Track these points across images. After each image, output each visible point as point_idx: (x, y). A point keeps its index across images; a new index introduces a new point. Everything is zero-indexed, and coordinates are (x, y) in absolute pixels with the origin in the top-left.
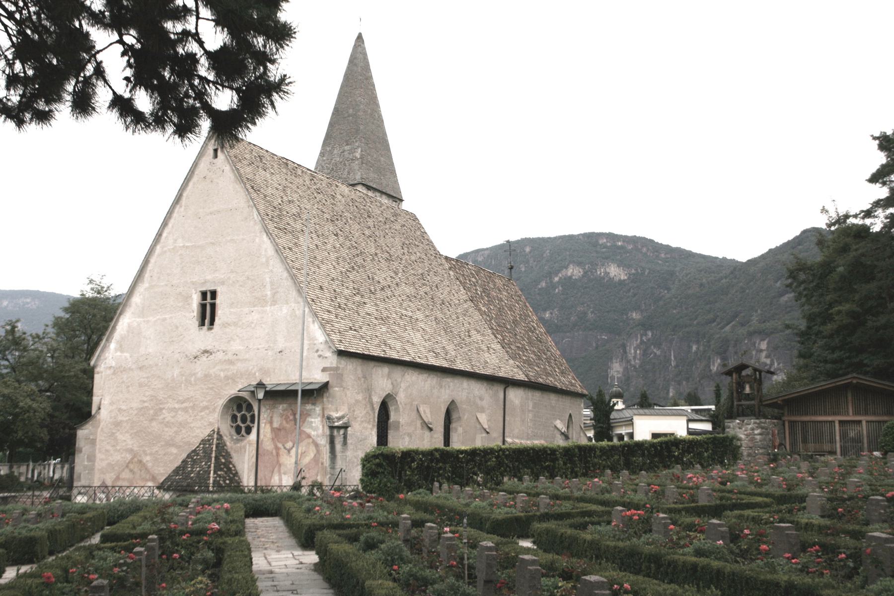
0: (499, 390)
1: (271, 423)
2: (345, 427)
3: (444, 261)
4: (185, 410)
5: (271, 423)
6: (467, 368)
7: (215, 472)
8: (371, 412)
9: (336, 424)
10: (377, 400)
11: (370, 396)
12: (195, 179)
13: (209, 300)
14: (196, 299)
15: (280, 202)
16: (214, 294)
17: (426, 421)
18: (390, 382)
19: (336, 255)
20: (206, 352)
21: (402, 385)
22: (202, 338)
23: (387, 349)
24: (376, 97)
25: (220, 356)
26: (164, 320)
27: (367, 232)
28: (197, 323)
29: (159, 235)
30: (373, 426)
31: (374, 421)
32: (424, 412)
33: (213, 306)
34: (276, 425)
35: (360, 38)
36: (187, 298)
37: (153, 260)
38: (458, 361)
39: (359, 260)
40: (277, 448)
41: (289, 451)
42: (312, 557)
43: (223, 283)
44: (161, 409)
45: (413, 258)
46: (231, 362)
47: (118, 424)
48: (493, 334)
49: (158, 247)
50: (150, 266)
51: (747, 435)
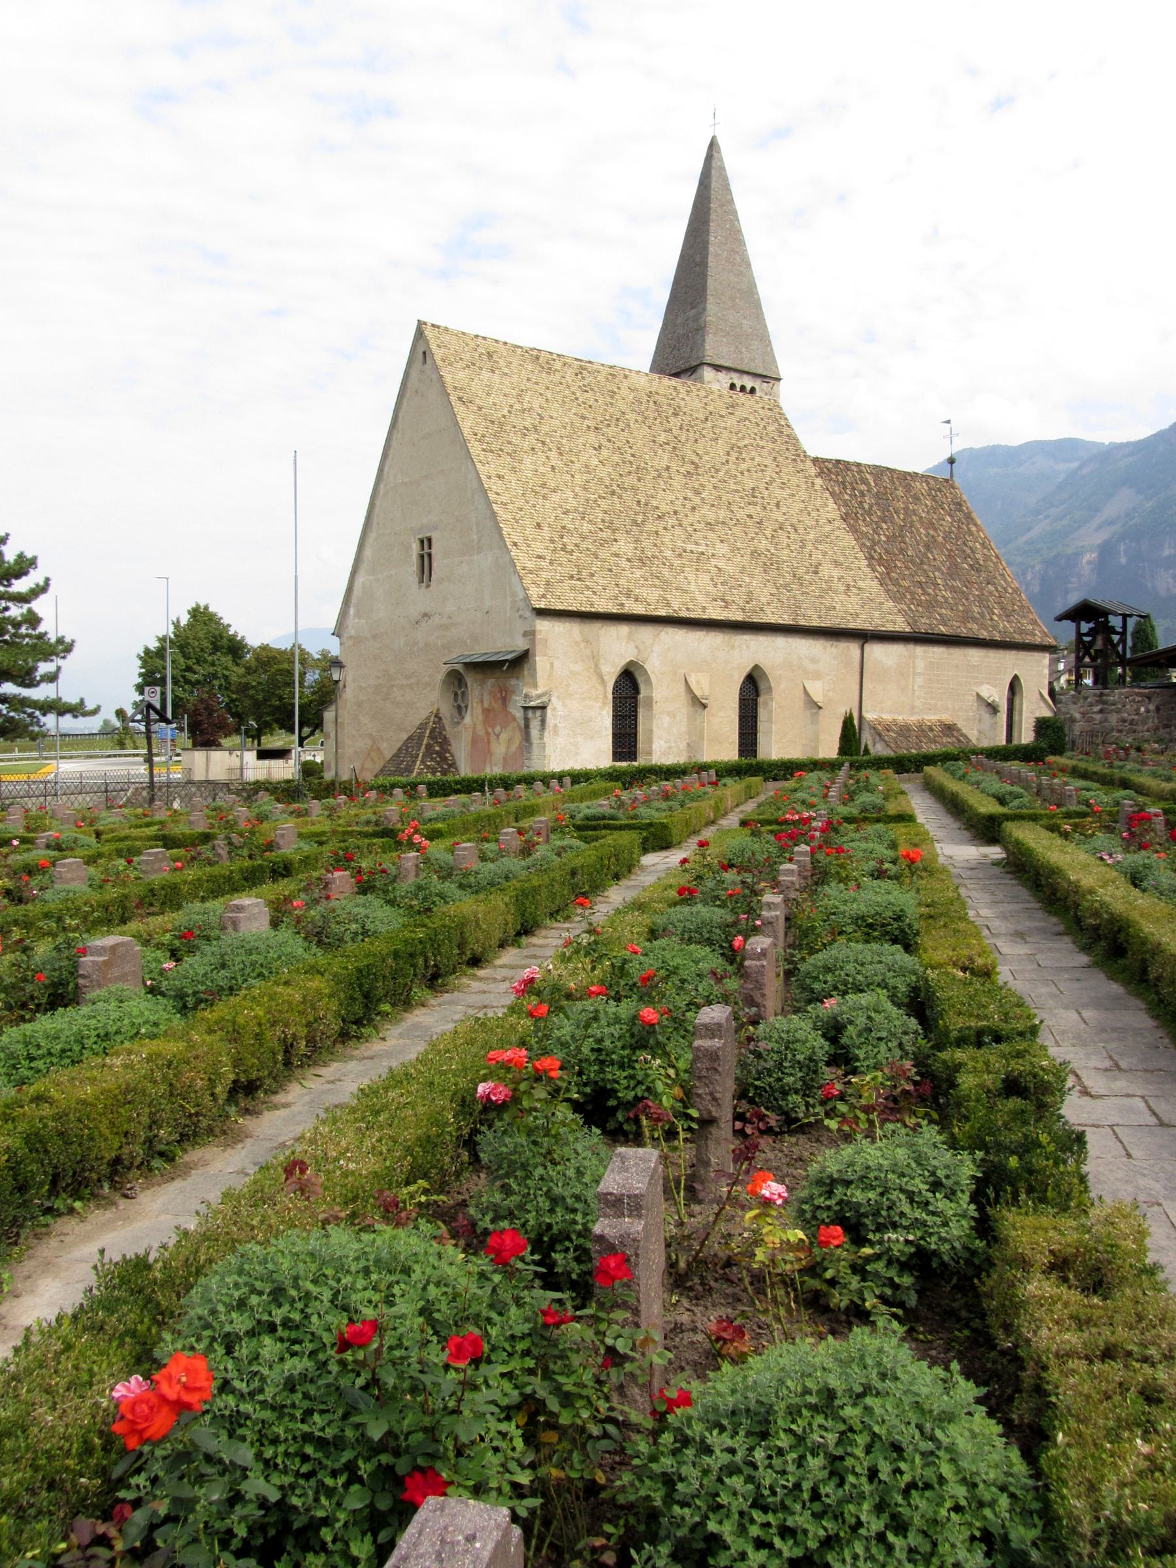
0: (852, 649)
1: (482, 702)
2: (543, 708)
3: (809, 464)
4: (411, 686)
5: (482, 702)
6: (786, 619)
7: (423, 762)
8: (600, 687)
9: (532, 704)
10: (611, 673)
11: (596, 666)
12: (408, 394)
13: (426, 550)
14: (415, 548)
15: (505, 412)
16: (430, 540)
17: (698, 693)
18: (631, 645)
19: (586, 477)
20: (425, 615)
21: (656, 648)
22: (419, 599)
23: (595, 599)
24: (740, 231)
25: (436, 619)
26: (390, 577)
27: (662, 438)
28: (417, 579)
29: (381, 470)
30: (604, 704)
31: (605, 696)
32: (698, 682)
33: (430, 555)
34: (486, 705)
35: (713, 146)
36: (408, 548)
37: (378, 503)
38: (768, 610)
39: (631, 480)
40: (488, 734)
41: (498, 736)
42: (995, 852)
43: (435, 528)
44: (392, 686)
45: (743, 466)
46: (446, 628)
47: (359, 705)
48: (869, 565)
49: (382, 486)
50: (377, 510)
51: (1083, 714)
